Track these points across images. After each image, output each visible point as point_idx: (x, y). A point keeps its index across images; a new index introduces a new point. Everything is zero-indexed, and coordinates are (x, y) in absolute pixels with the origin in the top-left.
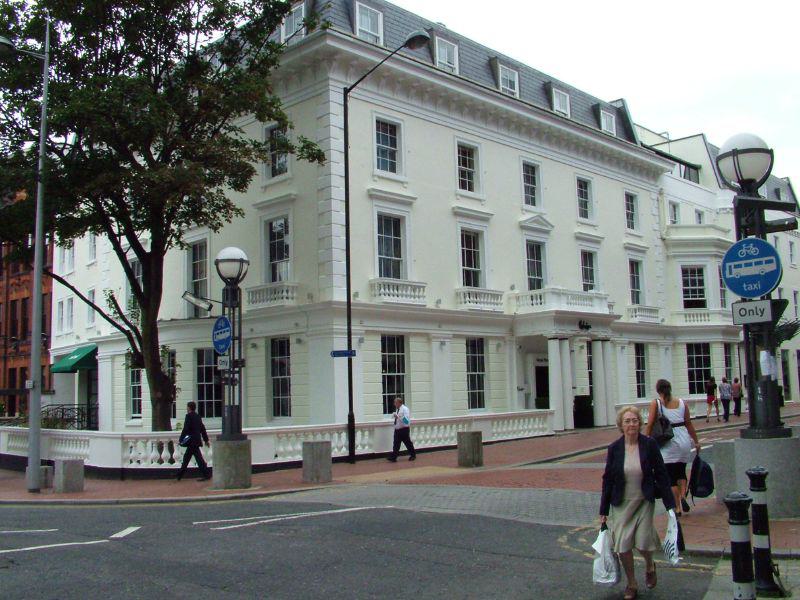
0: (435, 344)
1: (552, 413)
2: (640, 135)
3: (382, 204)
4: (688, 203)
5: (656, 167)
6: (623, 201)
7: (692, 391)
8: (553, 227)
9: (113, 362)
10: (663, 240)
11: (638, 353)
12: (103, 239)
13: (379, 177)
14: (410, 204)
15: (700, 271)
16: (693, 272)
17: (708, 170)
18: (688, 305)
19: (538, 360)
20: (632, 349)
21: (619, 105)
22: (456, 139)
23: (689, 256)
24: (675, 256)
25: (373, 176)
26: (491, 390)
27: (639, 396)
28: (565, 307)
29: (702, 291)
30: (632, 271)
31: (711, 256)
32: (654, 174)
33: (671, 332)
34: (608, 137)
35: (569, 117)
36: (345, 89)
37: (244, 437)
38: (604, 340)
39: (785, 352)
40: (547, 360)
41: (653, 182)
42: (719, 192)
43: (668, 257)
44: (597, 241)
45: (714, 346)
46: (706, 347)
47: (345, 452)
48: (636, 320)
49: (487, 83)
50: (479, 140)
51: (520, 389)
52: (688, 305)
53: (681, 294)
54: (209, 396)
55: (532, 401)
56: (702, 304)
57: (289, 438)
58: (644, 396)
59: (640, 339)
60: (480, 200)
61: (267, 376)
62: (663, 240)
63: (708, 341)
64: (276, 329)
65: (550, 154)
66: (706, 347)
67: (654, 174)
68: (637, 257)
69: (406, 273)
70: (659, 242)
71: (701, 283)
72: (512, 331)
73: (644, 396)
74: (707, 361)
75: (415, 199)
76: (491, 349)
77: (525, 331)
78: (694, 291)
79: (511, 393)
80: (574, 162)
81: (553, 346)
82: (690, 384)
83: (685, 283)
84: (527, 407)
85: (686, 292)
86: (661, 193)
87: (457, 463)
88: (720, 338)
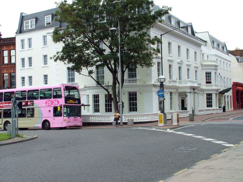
2: (196, 35)
3: (180, 65)
4: (206, 53)
5: (200, 43)
6: (194, 53)
7: (207, 107)
10: (201, 64)
14: (172, 62)
15: (210, 73)
16: (208, 73)
17: (209, 42)
18: (207, 83)
20: (169, 94)
21: (190, 24)
23: (209, 69)
24: (204, 69)
29: (210, 79)
31: (213, 69)
32: (199, 46)
33: (203, 90)
34: (172, 27)
35: (174, 26)
36: (161, 34)
39: (225, 96)
41: (199, 48)
42: (212, 49)
43: (202, 69)
46: (211, 95)
48: (170, 85)
49: (169, 23)
51: (179, 105)
52: (207, 83)
53: (205, 80)
54: (108, 107)
56: (210, 83)
59: (172, 91)
60: (171, 57)
61: (93, 103)
62: (201, 64)
63: (211, 93)
64: (132, 90)
65: (191, 46)
66: (211, 95)
67: (199, 46)
68: (171, 63)
69: (172, 77)
70: (200, 65)
71: (210, 77)
72: (177, 90)
74: (211, 98)
76: (173, 94)
77: (180, 91)
78: (208, 79)
79: (177, 106)
80: (194, 47)
82: (137, 106)
83: (206, 77)
84: (180, 110)
85: (206, 79)
86: (201, 51)
87: (189, 121)
88: (215, 92)
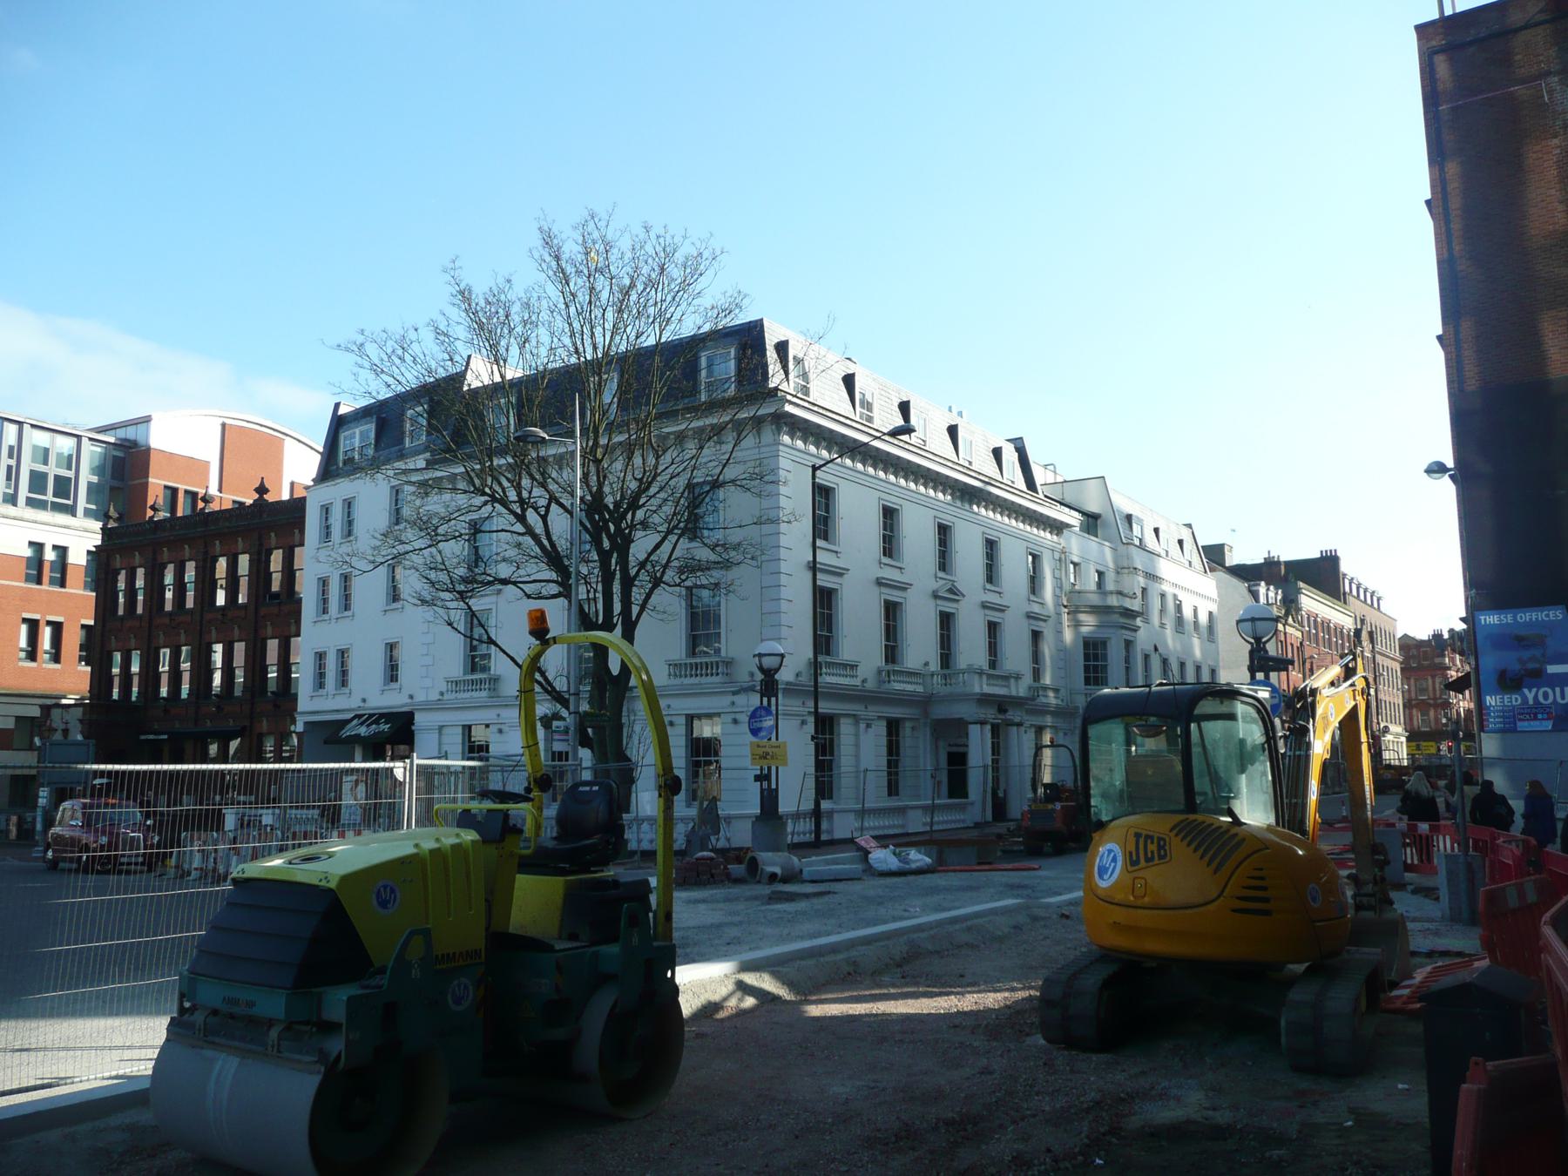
0: (862, 726)
1: (972, 804)
8: (964, 596)
9: (440, 734)
11: (889, 734)
12: (566, 602)
13: (885, 564)
19: (950, 745)
22: (882, 502)
25: (880, 563)
26: (905, 782)
27: (890, 794)
28: (987, 689)
30: (887, 617)
37: (781, 818)
38: (1019, 725)
40: (967, 746)
44: (903, 587)
45: (843, 721)
47: (810, 838)
50: (954, 519)
55: (945, 789)
57: (869, 814)
58: (897, 794)
73: (897, 794)
75: (848, 570)
76: (906, 730)
77: (941, 712)
81: (974, 730)
